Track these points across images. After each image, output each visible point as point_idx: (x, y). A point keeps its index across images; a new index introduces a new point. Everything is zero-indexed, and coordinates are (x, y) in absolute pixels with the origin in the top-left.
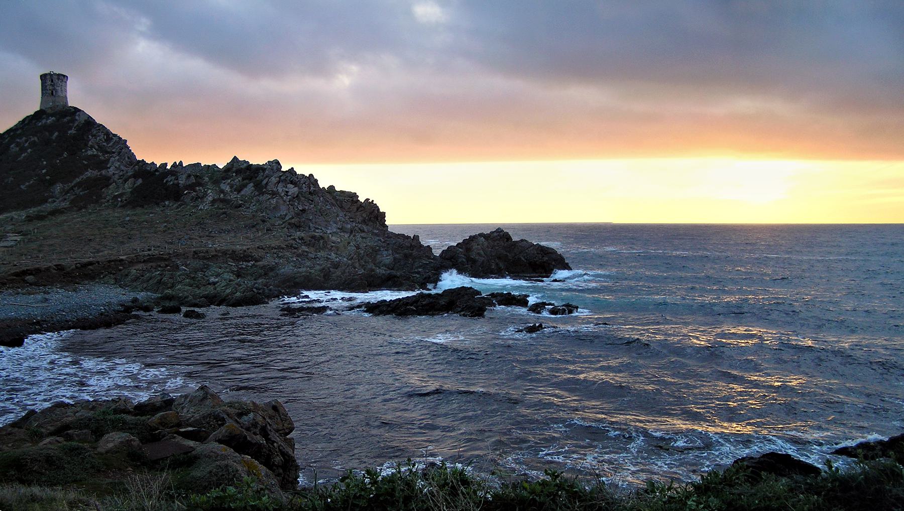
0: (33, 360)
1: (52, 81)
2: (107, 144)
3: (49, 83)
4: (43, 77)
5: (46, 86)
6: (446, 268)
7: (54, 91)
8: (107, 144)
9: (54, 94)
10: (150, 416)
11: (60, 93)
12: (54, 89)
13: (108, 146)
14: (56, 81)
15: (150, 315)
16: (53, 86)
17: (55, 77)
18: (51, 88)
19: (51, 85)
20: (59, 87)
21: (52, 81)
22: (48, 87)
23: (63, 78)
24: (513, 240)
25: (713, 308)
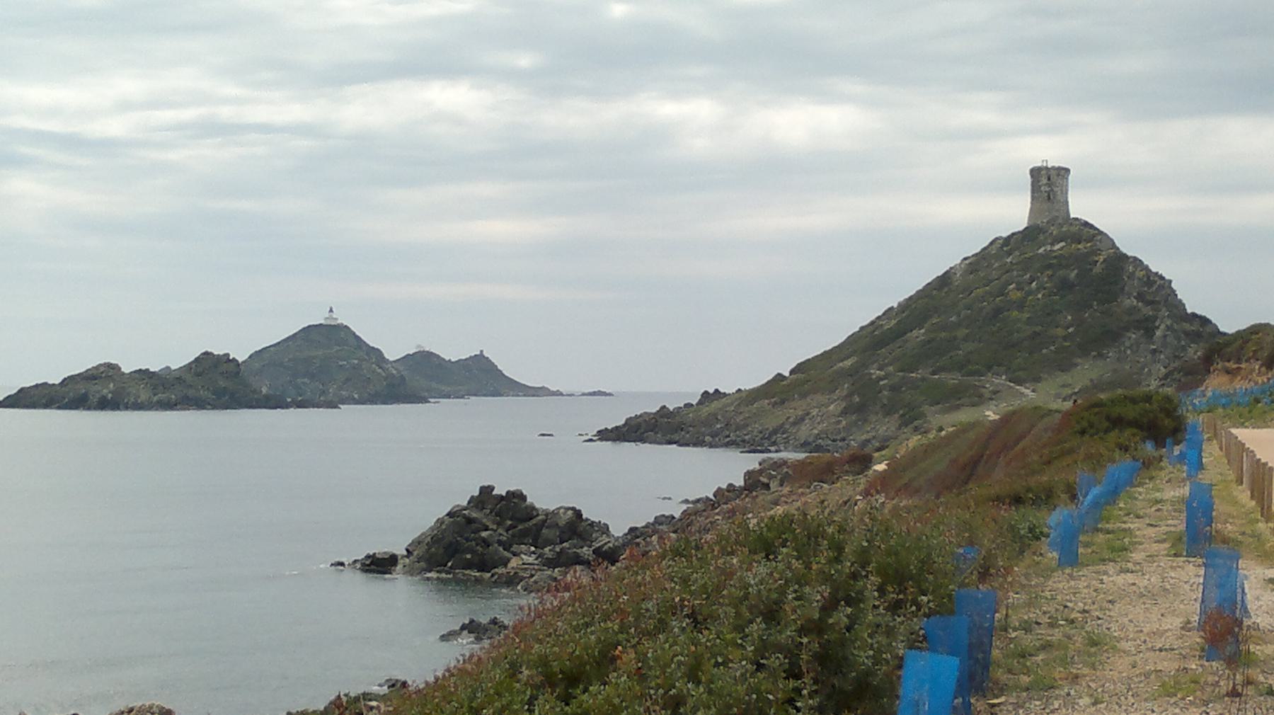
0: (791, 420)
1: (1049, 179)
2: (1149, 289)
3: (1044, 181)
4: (1036, 173)
5: (1040, 187)
6: (72, 401)
7: (1051, 194)
8: (1149, 289)
9: (1052, 197)
10: (553, 546)
11: (1059, 197)
12: (1052, 190)
13: (1150, 291)
14: (1054, 178)
15: (980, 381)
16: (1049, 186)
17: (1053, 173)
18: (1047, 189)
19: (1047, 184)
20: (1058, 187)
21: (1049, 179)
22: (1042, 188)
23: (1063, 172)
24: (958, 659)
25: (752, 462)
